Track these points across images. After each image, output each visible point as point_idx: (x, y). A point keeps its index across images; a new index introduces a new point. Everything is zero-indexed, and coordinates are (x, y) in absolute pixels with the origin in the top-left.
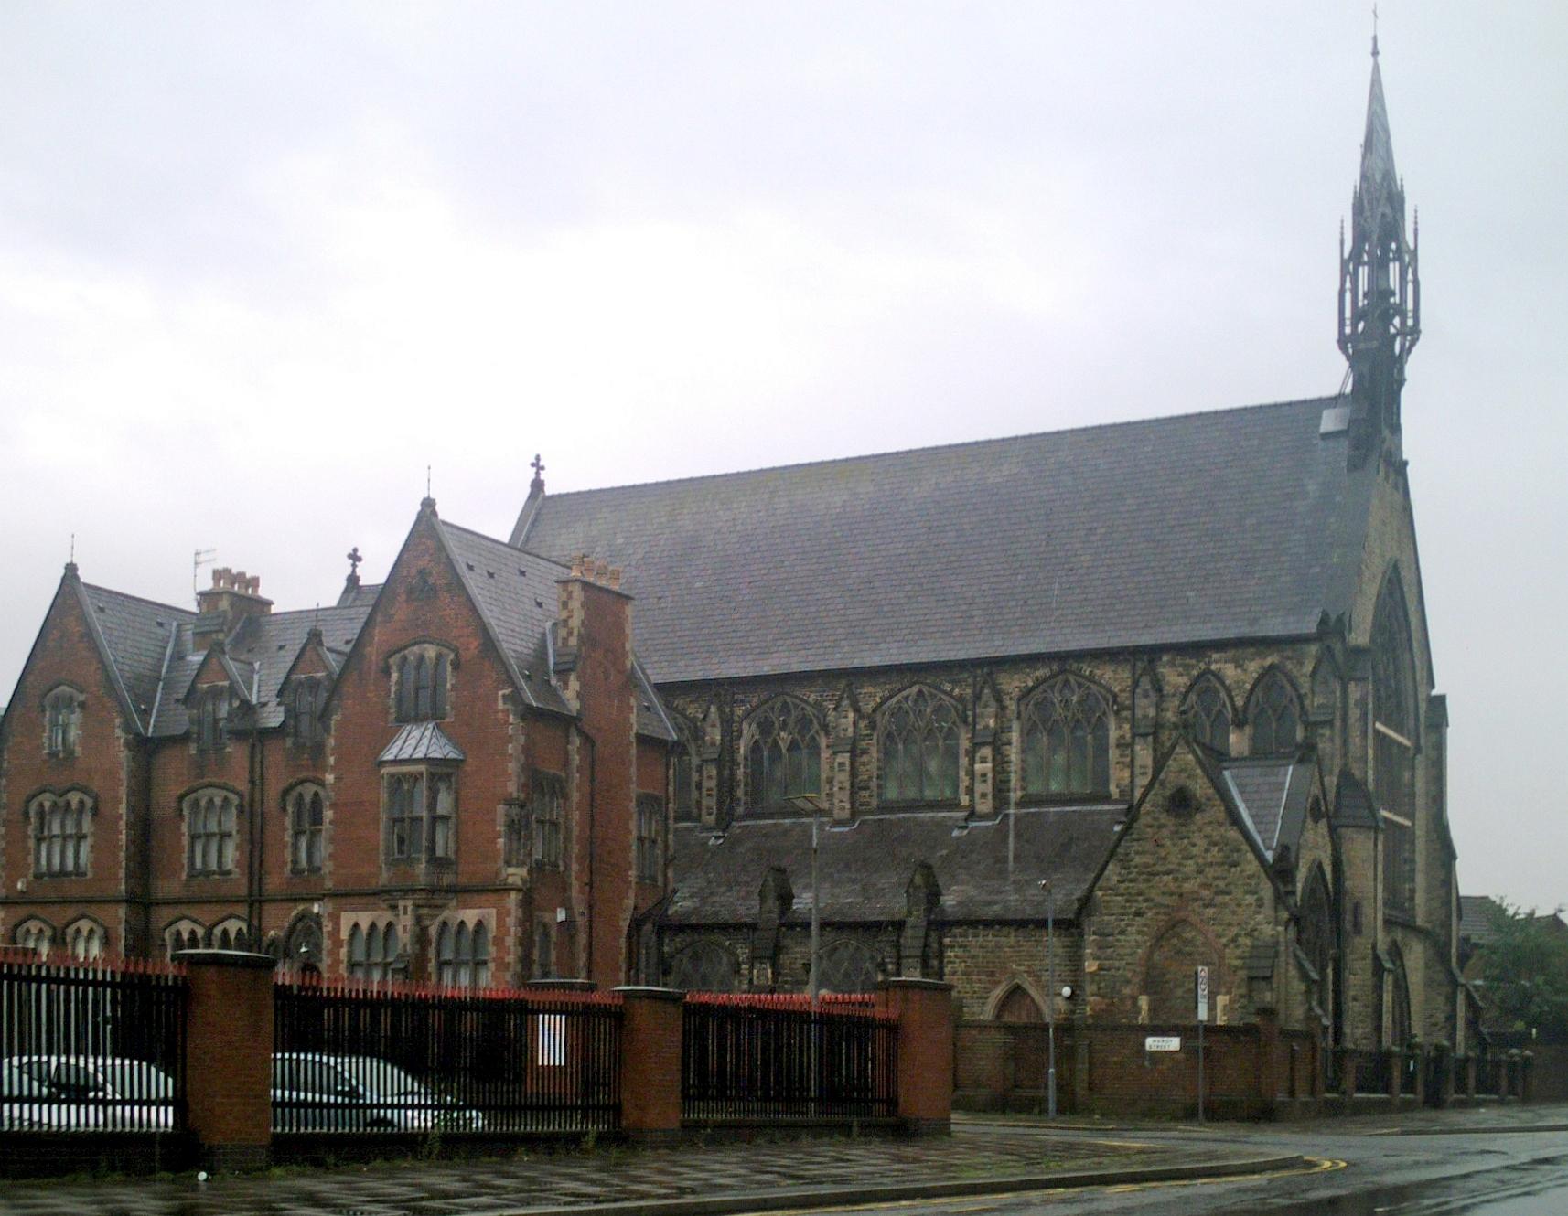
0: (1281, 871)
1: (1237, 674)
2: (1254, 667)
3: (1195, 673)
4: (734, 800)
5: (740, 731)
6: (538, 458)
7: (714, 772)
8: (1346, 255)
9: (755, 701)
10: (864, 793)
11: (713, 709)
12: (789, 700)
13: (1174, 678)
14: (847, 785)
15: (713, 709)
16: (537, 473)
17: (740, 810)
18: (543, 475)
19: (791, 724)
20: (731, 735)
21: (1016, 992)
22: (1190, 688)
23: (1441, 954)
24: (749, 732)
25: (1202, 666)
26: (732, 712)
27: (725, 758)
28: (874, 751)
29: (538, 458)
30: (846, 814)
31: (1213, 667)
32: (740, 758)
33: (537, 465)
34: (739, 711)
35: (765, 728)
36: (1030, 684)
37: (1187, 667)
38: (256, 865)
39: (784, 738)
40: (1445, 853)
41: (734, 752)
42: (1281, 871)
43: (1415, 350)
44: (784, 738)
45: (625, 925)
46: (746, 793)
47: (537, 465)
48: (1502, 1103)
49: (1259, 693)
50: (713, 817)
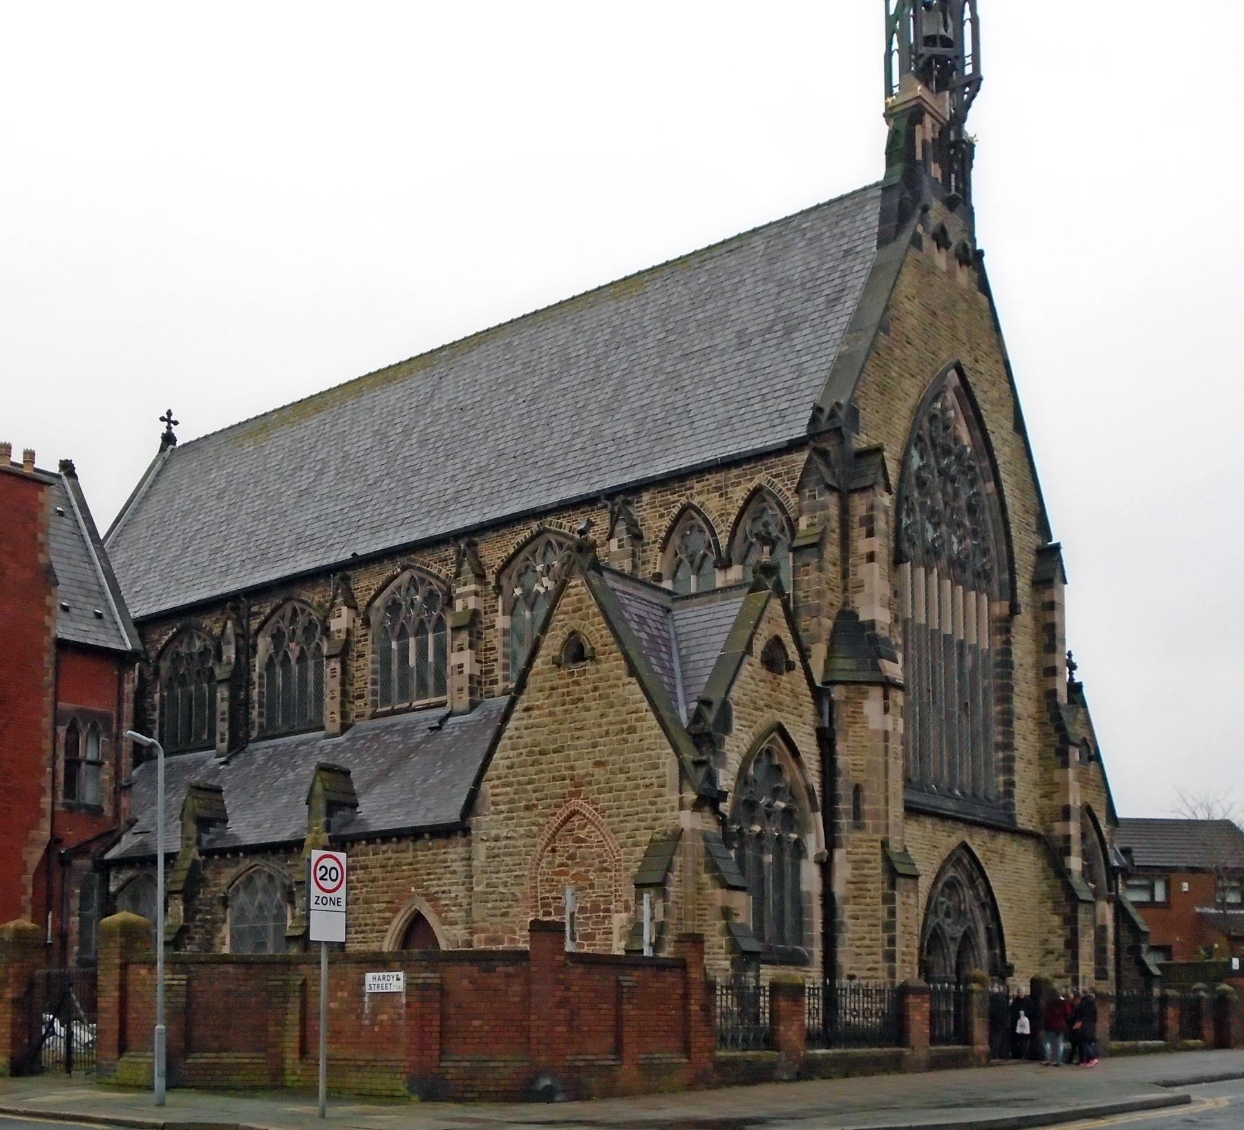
0: (704, 734)
1: (719, 504)
2: (739, 494)
3: (675, 511)
4: (248, 724)
5: (255, 647)
6: (169, 413)
7: (226, 694)
8: (892, 12)
9: (268, 610)
10: (359, 702)
11: (230, 624)
12: (298, 605)
13: (653, 516)
14: (337, 694)
15: (230, 624)
16: (169, 428)
17: (254, 734)
18: (175, 429)
19: (299, 632)
20: (246, 649)
21: (417, 920)
22: (670, 530)
23: (1053, 853)
24: (264, 644)
25: (684, 500)
26: (248, 625)
27: (239, 679)
28: (370, 657)
29: (169, 413)
30: (336, 728)
31: (695, 502)
32: (255, 676)
33: (168, 419)
34: (254, 625)
35: (277, 637)
36: (511, 551)
37: (668, 505)
38: (789, 919)
39: (294, 650)
40: (1065, 727)
41: (249, 669)
42: (704, 734)
43: (974, 102)
44: (294, 650)
45: (34, 856)
46: (261, 714)
47: (168, 419)
48: (1172, 1048)
49: (746, 524)
50: (225, 744)
